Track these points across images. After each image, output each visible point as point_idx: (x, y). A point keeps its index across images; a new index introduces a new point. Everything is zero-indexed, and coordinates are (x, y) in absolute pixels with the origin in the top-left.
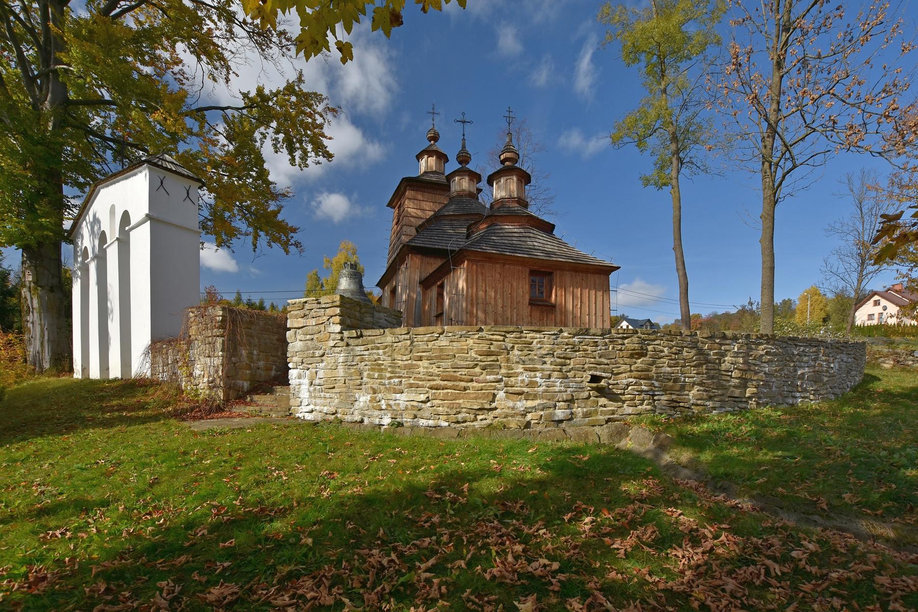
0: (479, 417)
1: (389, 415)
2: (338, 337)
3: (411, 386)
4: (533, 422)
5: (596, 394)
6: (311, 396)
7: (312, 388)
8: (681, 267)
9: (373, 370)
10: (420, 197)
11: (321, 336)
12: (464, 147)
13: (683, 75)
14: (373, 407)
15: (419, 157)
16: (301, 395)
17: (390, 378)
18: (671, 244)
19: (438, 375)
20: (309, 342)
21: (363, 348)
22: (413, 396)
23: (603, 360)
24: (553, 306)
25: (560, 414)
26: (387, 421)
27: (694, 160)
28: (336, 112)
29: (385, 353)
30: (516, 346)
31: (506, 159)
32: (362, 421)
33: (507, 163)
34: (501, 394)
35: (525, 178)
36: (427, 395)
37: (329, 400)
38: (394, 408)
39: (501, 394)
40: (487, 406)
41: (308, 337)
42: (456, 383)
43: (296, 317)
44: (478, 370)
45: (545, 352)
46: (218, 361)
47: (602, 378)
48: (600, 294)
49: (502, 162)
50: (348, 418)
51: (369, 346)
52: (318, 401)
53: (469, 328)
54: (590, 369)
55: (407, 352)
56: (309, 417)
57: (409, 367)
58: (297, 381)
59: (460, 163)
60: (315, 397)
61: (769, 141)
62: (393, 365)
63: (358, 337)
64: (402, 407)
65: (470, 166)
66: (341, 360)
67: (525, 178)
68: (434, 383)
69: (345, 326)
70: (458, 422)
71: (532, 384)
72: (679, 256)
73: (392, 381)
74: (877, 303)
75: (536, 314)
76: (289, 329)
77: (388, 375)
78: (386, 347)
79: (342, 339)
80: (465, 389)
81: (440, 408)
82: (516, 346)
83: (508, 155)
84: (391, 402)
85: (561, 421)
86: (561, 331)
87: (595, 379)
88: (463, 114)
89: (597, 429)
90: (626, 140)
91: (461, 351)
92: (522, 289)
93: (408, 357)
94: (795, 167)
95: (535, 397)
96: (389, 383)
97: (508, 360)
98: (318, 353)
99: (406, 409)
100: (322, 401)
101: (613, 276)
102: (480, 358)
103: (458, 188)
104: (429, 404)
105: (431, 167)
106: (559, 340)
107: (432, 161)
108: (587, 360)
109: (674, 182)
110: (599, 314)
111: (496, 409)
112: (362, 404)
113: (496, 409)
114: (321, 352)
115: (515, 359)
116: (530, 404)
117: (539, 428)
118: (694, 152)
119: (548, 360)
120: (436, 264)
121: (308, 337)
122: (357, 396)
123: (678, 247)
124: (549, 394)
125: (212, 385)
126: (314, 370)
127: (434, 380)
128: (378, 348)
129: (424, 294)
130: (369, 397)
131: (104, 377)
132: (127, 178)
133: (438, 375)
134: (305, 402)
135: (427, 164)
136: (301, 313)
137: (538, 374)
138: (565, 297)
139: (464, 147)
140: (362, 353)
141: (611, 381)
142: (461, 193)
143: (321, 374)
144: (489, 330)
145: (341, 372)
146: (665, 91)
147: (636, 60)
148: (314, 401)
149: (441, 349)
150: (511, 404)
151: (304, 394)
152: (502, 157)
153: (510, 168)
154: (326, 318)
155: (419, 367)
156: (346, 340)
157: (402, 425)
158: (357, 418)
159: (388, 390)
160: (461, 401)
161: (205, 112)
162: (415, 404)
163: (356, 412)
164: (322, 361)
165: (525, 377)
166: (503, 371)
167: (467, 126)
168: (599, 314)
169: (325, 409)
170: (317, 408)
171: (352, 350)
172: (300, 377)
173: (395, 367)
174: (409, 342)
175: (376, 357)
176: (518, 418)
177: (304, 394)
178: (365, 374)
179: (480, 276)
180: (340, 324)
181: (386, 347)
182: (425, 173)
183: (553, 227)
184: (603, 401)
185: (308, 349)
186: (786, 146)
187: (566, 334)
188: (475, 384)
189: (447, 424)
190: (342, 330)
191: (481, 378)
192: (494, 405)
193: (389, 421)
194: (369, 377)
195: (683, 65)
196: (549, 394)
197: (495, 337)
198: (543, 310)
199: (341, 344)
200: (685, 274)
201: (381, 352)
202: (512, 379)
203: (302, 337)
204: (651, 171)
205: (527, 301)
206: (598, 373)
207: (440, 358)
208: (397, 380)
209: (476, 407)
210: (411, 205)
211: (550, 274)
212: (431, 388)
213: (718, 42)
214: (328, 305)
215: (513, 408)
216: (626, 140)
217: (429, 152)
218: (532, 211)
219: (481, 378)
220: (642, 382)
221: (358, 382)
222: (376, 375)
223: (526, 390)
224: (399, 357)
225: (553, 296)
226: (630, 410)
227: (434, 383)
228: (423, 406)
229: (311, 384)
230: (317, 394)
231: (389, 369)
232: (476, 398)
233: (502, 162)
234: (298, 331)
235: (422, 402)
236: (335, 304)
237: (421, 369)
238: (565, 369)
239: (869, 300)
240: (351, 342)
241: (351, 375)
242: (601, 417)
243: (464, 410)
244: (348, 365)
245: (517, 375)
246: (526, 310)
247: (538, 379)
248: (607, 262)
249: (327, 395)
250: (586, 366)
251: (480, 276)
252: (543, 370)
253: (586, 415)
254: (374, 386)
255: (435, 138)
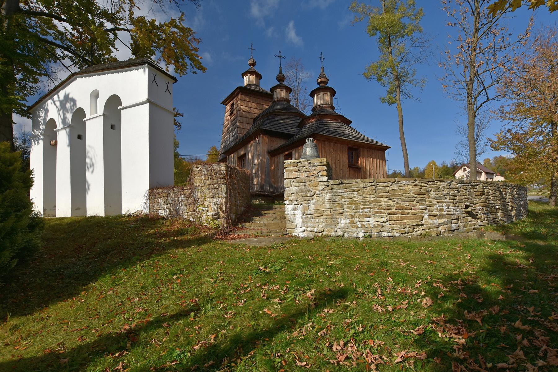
0: (415, 230)
1: (363, 231)
2: (326, 184)
3: (377, 213)
4: (442, 231)
5: (467, 215)
6: (303, 222)
7: (304, 217)
8: (404, 148)
9: (350, 204)
10: (247, 99)
11: (313, 183)
12: (281, 71)
13: (402, 45)
14: (352, 227)
15: (244, 75)
16: (296, 221)
17: (363, 209)
18: (399, 136)
19: (394, 206)
20: (303, 188)
21: (343, 191)
22: (377, 219)
23: (469, 197)
24: (360, 168)
25: (454, 226)
26: (361, 234)
27: (404, 91)
28: (199, 42)
29: (358, 194)
30: (433, 189)
31: (322, 82)
32: (343, 235)
33: (322, 84)
34: (426, 216)
35: (333, 93)
36: (386, 218)
37: (318, 224)
38: (366, 226)
39: (426, 216)
40: (420, 223)
41: (302, 184)
42: (403, 211)
43: (292, 171)
44: (414, 203)
45: (446, 193)
46: (222, 200)
47: (469, 206)
48: (381, 161)
49: (319, 84)
50: (333, 234)
51: (348, 190)
52: (309, 224)
53: (410, 179)
54: (465, 202)
55: (373, 193)
56: (302, 235)
57: (375, 202)
58: (292, 212)
59: (279, 81)
60: (307, 222)
61: (470, 86)
62: (364, 201)
63: (339, 184)
64: (372, 225)
65: (285, 83)
66: (327, 198)
67: (333, 93)
68: (391, 211)
69: (330, 177)
70: (405, 233)
71: (441, 210)
72: (403, 142)
73: (365, 210)
74: (465, 170)
75: (352, 172)
76: (286, 179)
77: (362, 207)
78: (359, 190)
79: (328, 186)
80: (408, 214)
81: (395, 226)
82: (433, 189)
83: (323, 79)
84: (364, 223)
85: (454, 230)
86: (452, 181)
87: (467, 207)
88: (280, 52)
89: (470, 233)
90: (373, 77)
91: (406, 192)
92: (344, 158)
93: (374, 196)
94: (488, 100)
95: (440, 217)
96: (362, 212)
97: (429, 197)
98: (309, 194)
99: (374, 226)
100: (312, 224)
101: (386, 152)
102: (416, 196)
103: (279, 96)
104: (387, 223)
105: (252, 81)
106: (451, 186)
107: (253, 78)
108: (464, 197)
109: (398, 102)
110: (381, 173)
111: (423, 225)
112: (343, 225)
113: (423, 225)
114: (312, 193)
115: (432, 196)
116: (441, 221)
117: (445, 234)
118: (406, 87)
119: (448, 197)
120: (279, 143)
121: (302, 184)
122: (339, 220)
123: (402, 138)
124: (449, 216)
125: (216, 217)
126: (307, 205)
127: (391, 209)
128: (354, 191)
129: (271, 160)
130: (348, 221)
131: (113, 214)
132: (116, 73)
133: (394, 206)
134: (299, 225)
135: (248, 79)
136: (296, 169)
137: (444, 205)
138: (367, 163)
139: (281, 71)
140: (343, 194)
141: (473, 208)
142: (282, 99)
143: (312, 207)
144: (420, 180)
145: (327, 205)
146: (391, 52)
147: (374, 34)
148: (306, 225)
149: (394, 191)
150: (431, 222)
151: (298, 219)
152: (319, 81)
153: (323, 87)
154: (315, 172)
155: (381, 201)
156: (330, 186)
157: (371, 237)
158: (340, 233)
159: (362, 216)
160: (406, 221)
161: (117, 31)
162: (379, 223)
163: (339, 230)
164: (313, 199)
165: (437, 206)
166: (427, 203)
167: (282, 59)
168: (381, 173)
169: (315, 230)
170: (309, 229)
171: (335, 192)
172: (295, 209)
173: (366, 202)
174: (374, 187)
175: (352, 196)
176: (435, 229)
177: (298, 219)
178: (345, 206)
179: (323, 150)
180: (327, 176)
181: (359, 190)
182: (249, 85)
183: (351, 122)
184: (470, 219)
185: (302, 191)
186: (484, 87)
187: (454, 183)
188: (413, 211)
189: (399, 235)
190: (328, 179)
191: (416, 207)
192: (423, 222)
193: (363, 234)
194: (348, 208)
195: (400, 40)
196: (449, 216)
197: (422, 184)
198: (357, 171)
199: (328, 188)
200: (407, 152)
201: (356, 193)
202: (431, 208)
203: (295, 184)
204: (386, 96)
205: (347, 165)
206: (469, 204)
207: (395, 196)
208: (368, 210)
209: (414, 224)
210: (243, 104)
211: (358, 149)
212: (389, 214)
213: (421, 31)
214: (317, 164)
215: (433, 224)
216: (373, 77)
217: (252, 73)
218: (337, 111)
219: (416, 207)
220: (484, 208)
221: (341, 211)
222: (353, 207)
223: (438, 213)
224: (368, 196)
225: (359, 162)
226: (481, 223)
227: (391, 211)
228: (384, 224)
229: (304, 214)
230: (309, 220)
231: (362, 203)
232: (413, 219)
233: (319, 84)
234: (292, 180)
235: (383, 222)
236: (323, 164)
237: (383, 203)
238: (455, 201)
239: (461, 168)
240: (334, 187)
241: (335, 207)
242: (470, 228)
243: (408, 226)
244: (332, 201)
245: (434, 205)
246: (347, 170)
247: (444, 208)
248: (384, 144)
249: (317, 220)
250: (463, 200)
251: (323, 150)
252: (446, 202)
253: (465, 226)
254: (352, 214)
255: (254, 64)
